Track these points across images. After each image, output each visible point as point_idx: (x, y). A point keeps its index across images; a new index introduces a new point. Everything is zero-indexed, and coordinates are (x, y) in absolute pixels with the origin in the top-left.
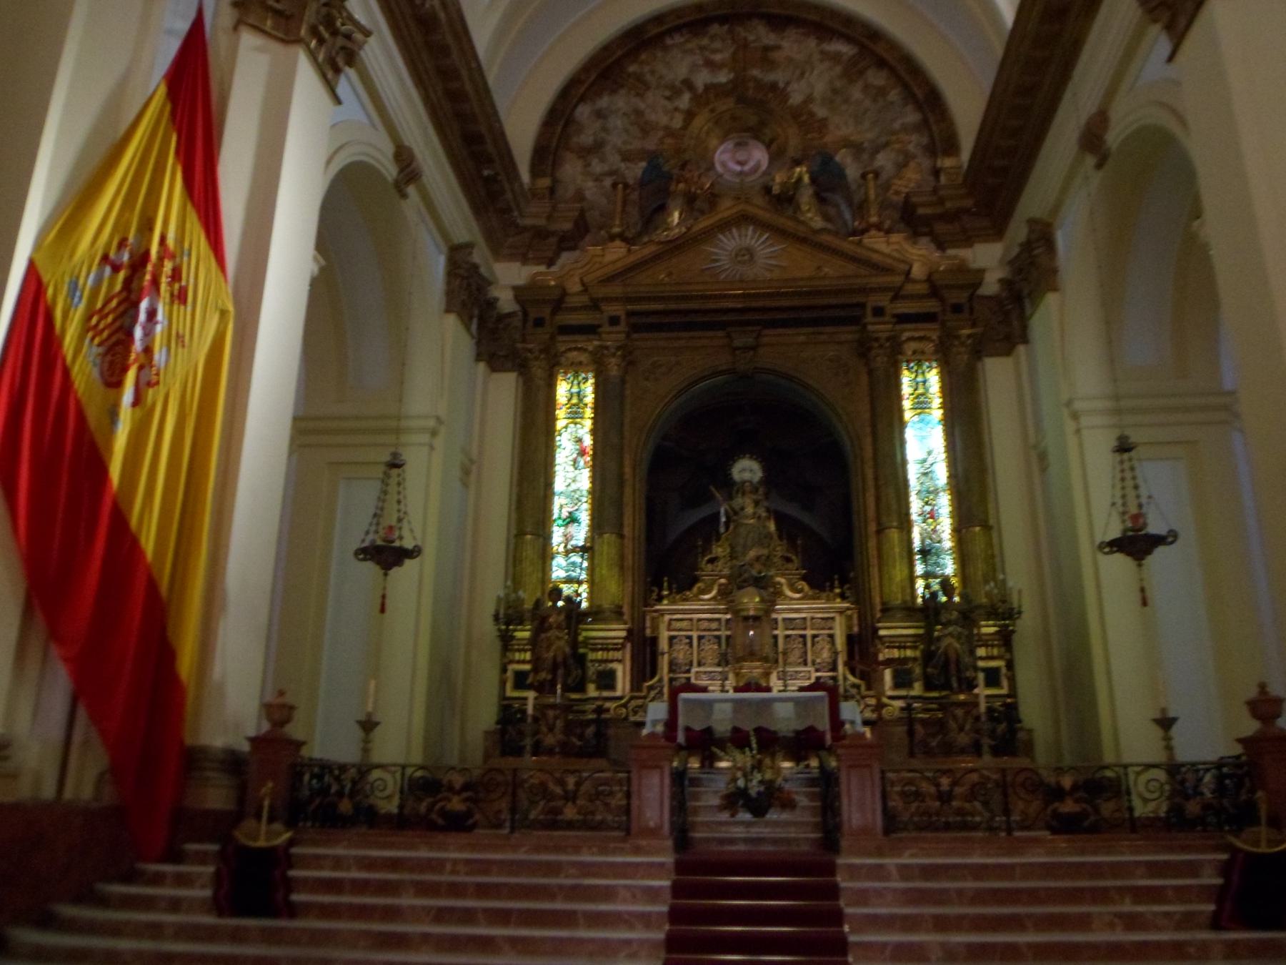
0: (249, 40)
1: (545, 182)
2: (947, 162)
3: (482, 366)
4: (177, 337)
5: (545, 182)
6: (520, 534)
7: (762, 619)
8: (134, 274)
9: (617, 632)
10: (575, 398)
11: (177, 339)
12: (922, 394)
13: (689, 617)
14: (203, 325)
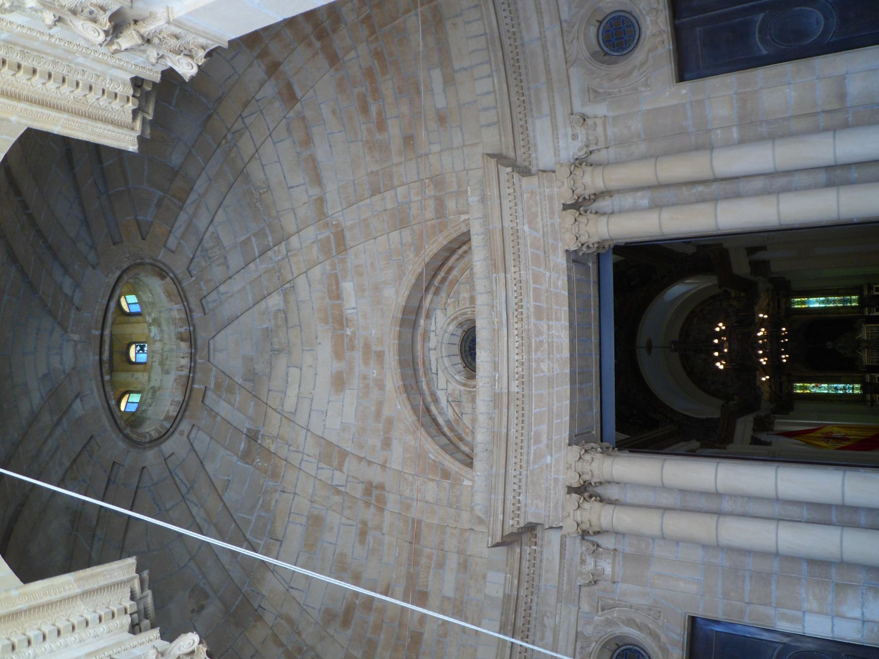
0: (775, 428)
1: (736, 397)
2: (733, 295)
3: (791, 413)
4: (838, 432)
5: (736, 397)
6: (840, 401)
7: (867, 341)
8: (828, 437)
9: (868, 377)
10: (799, 388)
11: (839, 432)
12: (798, 303)
13: (866, 358)
14: (836, 429)
